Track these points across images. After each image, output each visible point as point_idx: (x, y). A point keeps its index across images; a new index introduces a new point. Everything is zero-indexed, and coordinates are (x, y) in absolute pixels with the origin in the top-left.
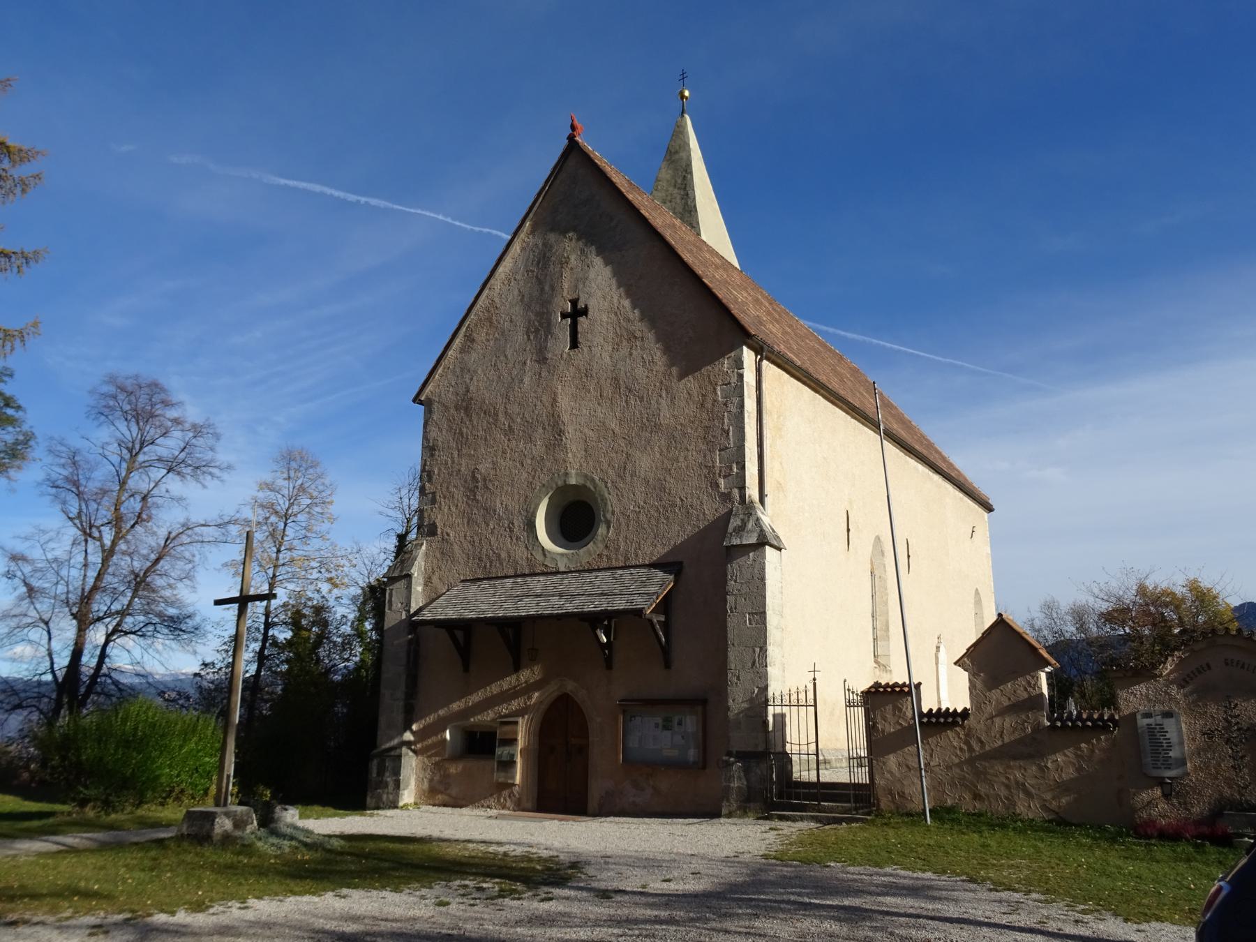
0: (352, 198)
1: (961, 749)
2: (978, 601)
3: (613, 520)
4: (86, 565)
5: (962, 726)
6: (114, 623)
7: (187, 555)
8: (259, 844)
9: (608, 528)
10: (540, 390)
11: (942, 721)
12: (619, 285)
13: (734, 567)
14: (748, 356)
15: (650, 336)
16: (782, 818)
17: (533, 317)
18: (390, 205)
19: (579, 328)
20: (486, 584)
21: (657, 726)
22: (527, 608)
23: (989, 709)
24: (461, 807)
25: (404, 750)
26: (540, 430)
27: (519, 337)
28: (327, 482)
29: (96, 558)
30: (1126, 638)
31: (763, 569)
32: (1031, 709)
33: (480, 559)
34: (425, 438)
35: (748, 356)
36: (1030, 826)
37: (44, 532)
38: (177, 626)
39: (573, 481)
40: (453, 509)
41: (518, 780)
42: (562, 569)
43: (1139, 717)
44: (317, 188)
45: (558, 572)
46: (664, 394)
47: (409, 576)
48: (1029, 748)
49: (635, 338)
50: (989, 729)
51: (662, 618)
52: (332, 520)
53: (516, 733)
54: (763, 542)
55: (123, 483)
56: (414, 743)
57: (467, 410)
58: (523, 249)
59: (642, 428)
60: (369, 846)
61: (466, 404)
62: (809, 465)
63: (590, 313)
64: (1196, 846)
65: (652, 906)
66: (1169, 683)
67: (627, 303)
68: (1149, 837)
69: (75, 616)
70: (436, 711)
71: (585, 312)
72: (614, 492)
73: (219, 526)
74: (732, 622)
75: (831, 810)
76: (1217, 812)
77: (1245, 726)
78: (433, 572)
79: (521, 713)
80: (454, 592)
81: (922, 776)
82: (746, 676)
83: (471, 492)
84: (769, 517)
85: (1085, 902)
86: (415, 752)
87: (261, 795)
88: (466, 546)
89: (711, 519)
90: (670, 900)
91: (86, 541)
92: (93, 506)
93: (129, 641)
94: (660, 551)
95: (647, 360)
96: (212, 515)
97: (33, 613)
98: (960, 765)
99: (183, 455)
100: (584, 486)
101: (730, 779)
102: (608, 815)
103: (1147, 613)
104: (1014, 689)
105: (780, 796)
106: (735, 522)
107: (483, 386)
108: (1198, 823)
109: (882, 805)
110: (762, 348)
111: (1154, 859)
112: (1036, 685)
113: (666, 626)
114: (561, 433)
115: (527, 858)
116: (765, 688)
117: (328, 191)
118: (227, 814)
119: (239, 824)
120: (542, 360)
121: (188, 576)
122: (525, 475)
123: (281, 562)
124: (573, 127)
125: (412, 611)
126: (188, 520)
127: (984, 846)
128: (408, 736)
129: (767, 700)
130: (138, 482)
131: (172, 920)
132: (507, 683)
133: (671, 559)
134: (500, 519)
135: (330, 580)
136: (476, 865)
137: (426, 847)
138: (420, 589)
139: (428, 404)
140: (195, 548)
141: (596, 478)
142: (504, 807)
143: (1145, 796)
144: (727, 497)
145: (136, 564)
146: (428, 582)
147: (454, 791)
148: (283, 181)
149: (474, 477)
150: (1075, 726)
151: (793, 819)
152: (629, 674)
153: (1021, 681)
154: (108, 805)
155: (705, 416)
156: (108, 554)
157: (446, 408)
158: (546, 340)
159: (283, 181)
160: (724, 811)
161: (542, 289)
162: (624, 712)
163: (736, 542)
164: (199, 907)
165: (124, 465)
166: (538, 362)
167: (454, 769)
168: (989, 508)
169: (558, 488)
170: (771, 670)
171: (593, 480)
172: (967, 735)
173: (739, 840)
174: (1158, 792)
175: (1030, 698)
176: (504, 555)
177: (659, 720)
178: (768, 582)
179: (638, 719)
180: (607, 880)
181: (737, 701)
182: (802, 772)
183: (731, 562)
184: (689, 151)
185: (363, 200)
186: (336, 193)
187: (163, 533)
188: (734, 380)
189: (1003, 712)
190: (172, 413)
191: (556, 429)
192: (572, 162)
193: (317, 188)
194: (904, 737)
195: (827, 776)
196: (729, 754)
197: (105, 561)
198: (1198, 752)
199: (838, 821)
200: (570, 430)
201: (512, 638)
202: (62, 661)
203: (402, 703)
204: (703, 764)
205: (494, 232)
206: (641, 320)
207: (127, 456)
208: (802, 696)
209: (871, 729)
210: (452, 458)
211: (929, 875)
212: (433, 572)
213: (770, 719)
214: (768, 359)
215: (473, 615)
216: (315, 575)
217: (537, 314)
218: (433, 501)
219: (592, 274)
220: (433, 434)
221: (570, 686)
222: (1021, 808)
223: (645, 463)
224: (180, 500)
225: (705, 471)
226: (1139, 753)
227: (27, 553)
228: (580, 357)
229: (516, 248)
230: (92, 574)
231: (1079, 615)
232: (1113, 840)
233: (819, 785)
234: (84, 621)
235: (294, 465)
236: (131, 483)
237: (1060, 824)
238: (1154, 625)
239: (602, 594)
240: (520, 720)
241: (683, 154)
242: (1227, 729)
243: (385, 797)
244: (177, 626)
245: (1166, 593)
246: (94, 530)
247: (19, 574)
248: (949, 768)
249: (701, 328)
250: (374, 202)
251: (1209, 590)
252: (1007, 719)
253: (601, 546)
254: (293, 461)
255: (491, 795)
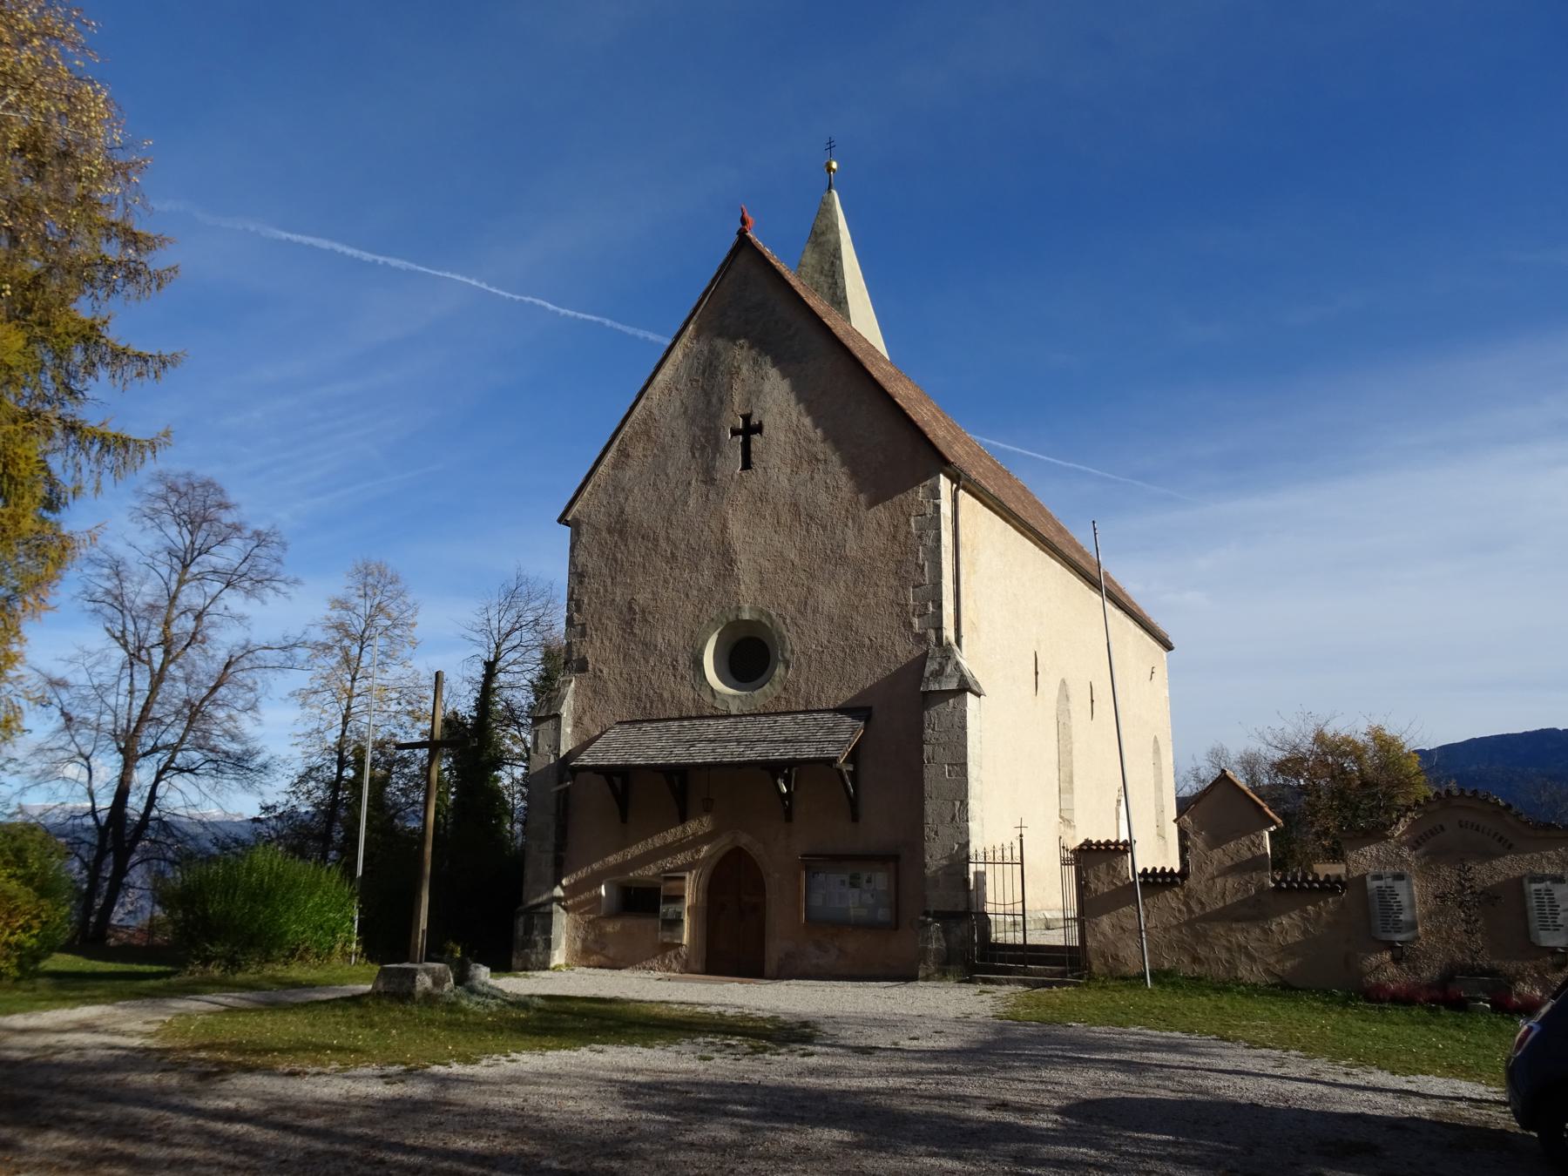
0: (367, 257)
1: (1180, 911)
2: (1157, 751)
3: (793, 659)
4: (131, 692)
5: (1182, 887)
6: (166, 759)
7: (249, 682)
8: (464, 1002)
9: (787, 668)
10: (707, 514)
11: (1156, 881)
12: (799, 400)
13: (931, 714)
14: (945, 484)
15: (835, 459)
16: (985, 981)
17: (698, 433)
18: (413, 266)
19: (753, 448)
20: (647, 727)
21: (843, 882)
22: (703, 754)
23: (1210, 869)
24: (620, 969)
25: (555, 906)
26: (708, 559)
27: (682, 454)
28: (410, 600)
29: (143, 683)
30: (1302, 790)
31: (964, 717)
32: (1255, 870)
33: (639, 699)
34: (572, 563)
35: (945, 484)
36: (1253, 990)
37: (90, 654)
38: (241, 764)
39: (746, 616)
40: (607, 643)
41: (685, 940)
42: (734, 712)
43: (1368, 879)
44: (325, 244)
45: (729, 716)
46: (850, 523)
47: (558, 717)
48: (1253, 910)
49: (818, 460)
50: (1209, 890)
51: (851, 768)
52: (414, 644)
53: (683, 889)
54: (965, 687)
55: (173, 599)
56: (564, 899)
57: (621, 533)
58: (685, 355)
59: (826, 559)
60: (575, 1007)
61: (620, 527)
62: (1004, 601)
63: (765, 431)
64: (1430, 1010)
65: (920, 1060)
66: (1401, 844)
67: (807, 421)
68: (1382, 1001)
69: (121, 750)
70: (589, 864)
71: (759, 429)
72: (793, 629)
73: (283, 649)
74: (929, 773)
75: (1039, 973)
76: (1450, 975)
77: (1478, 889)
78: (584, 712)
79: (689, 867)
80: (611, 734)
81: (1137, 938)
82: (945, 831)
83: (628, 625)
84: (970, 659)
85: (1345, 1058)
86: (565, 908)
87: (453, 951)
88: (623, 685)
89: (904, 661)
90: (936, 1055)
91: (132, 664)
92: (143, 625)
93: (179, 781)
94: (846, 695)
95: (831, 487)
96: (273, 634)
97: (73, 747)
98: (1178, 927)
99: (244, 568)
100: (759, 622)
101: (927, 940)
102: (789, 978)
103: (1325, 764)
104: (1239, 849)
105: (982, 958)
106: (931, 666)
107: (638, 507)
108: (1429, 987)
109: (1094, 968)
110: (959, 477)
111: (1390, 1022)
112: (1261, 845)
113: (853, 775)
114: (732, 562)
115: (774, 1019)
116: (966, 845)
117: (339, 248)
118: (427, 971)
119: (438, 981)
120: (709, 479)
121: (253, 707)
122: (690, 608)
123: (356, 691)
124: (743, 221)
125: (563, 751)
126: (248, 642)
127: (1218, 1008)
128: (558, 892)
129: (968, 857)
130: (191, 596)
131: (468, 1070)
132: (672, 835)
133: (858, 704)
134: (662, 655)
135: (409, 713)
136: (706, 1025)
137: (614, 1007)
138: (569, 730)
139: (575, 526)
140: (257, 675)
141: (773, 613)
142: (669, 969)
143: (1373, 960)
144: (921, 638)
145: (193, 693)
146: (578, 723)
147: (611, 952)
148: (285, 235)
149: (630, 609)
150: (1301, 887)
151: (999, 983)
152: (836, 825)
153: (1245, 840)
154: (233, 963)
155: (896, 548)
156: (158, 679)
157: (597, 530)
158: (714, 458)
159: (285, 235)
160: (921, 974)
161: (709, 402)
162: (807, 869)
163: (934, 687)
164: (467, 1060)
165: (175, 577)
166: (705, 482)
167: (611, 928)
168: (1168, 646)
169: (729, 623)
170: (973, 826)
171: (769, 616)
172: (1186, 896)
173: (943, 1007)
174: (1387, 956)
175: (1255, 858)
176: (666, 695)
177: (846, 878)
178: (969, 731)
179: (821, 877)
180: (849, 1036)
181: (935, 857)
182: (1002, 934)
183: (927, 708)
184: (838, 233)
185: (381, 259)
186: (349, 251)
187: (222, 655)
188: (930, 511)
189: (1225, 872)
190: (228, 517)
191: (728, 559)
192: (742, 259)
193: (325, 244)
194: (1124, 895)
195: (1036, 938)
196: (927, 914)
197: (154, 688)
198: (1430, 915)
199: (1049, 985)
200: (743, 561)
201: (678, 788)
202: (105, 802)
203: (551, 856)
204: (895, 925)
205: (538, 301)
206: (824, 440)
207: (178, 567)
208: (1007, 853)
209: (1082, 888)
210: (605, 586)
211: (1177, 1034)
212: (584, 712)
213: (972, 877)
214: (965, 489)
215: (640, 761)
216: (394, 707)
217: (703, 429)
218: (583, 634)
219: (767, 387)
220: (581, 559)
221: (744, 840)
222: (1243, 972)
223: (829, 598)
224: (241, 618)
225: (897, 609)
226: (1366, 913)
227: (71, 679)
228: (754, 479)
229: (678, 353)
230: (140, 702)
231: (1250, 764)
232: (1345, 1004)
233: (1025, 947)
234: (130, 759)
235: (370, 580)
236: (183, 600)
237: (1284, 988)
238: (1333, 777)
239: (785, 741)
240: (687, 875)
241: (831, 237)
242: (1460, 892)
243: (533, 958)
244: (241, 764)
245: (1346, 741)
246: (143, 652)
247: (56, 701)
248: (1166, 930)
249: (894, 455)
250: (394, 262)
251: (1395, 739)
252: (1230, 880)
253: (779, 688)
254: (373, 579)
255: (654, 956)
